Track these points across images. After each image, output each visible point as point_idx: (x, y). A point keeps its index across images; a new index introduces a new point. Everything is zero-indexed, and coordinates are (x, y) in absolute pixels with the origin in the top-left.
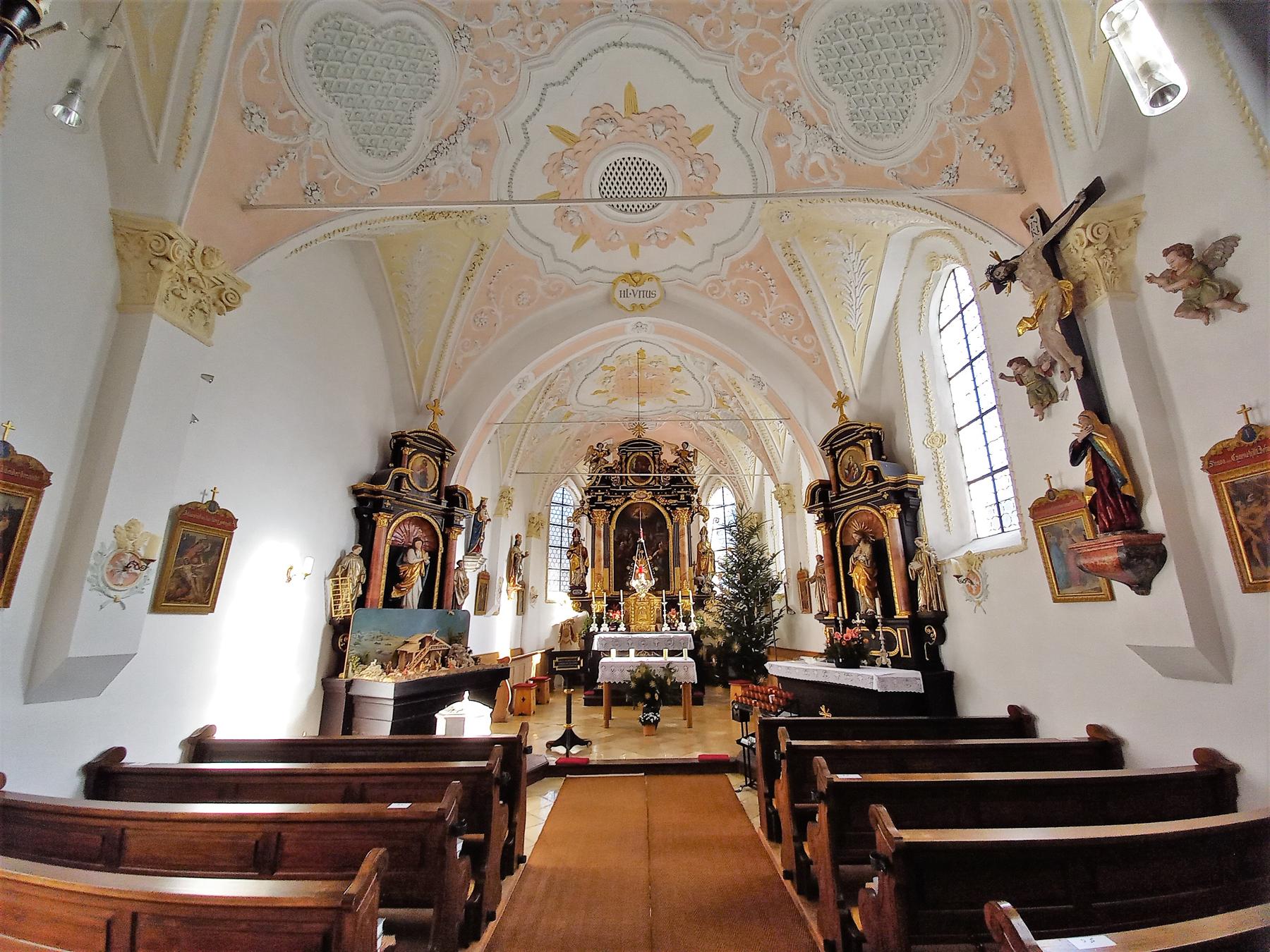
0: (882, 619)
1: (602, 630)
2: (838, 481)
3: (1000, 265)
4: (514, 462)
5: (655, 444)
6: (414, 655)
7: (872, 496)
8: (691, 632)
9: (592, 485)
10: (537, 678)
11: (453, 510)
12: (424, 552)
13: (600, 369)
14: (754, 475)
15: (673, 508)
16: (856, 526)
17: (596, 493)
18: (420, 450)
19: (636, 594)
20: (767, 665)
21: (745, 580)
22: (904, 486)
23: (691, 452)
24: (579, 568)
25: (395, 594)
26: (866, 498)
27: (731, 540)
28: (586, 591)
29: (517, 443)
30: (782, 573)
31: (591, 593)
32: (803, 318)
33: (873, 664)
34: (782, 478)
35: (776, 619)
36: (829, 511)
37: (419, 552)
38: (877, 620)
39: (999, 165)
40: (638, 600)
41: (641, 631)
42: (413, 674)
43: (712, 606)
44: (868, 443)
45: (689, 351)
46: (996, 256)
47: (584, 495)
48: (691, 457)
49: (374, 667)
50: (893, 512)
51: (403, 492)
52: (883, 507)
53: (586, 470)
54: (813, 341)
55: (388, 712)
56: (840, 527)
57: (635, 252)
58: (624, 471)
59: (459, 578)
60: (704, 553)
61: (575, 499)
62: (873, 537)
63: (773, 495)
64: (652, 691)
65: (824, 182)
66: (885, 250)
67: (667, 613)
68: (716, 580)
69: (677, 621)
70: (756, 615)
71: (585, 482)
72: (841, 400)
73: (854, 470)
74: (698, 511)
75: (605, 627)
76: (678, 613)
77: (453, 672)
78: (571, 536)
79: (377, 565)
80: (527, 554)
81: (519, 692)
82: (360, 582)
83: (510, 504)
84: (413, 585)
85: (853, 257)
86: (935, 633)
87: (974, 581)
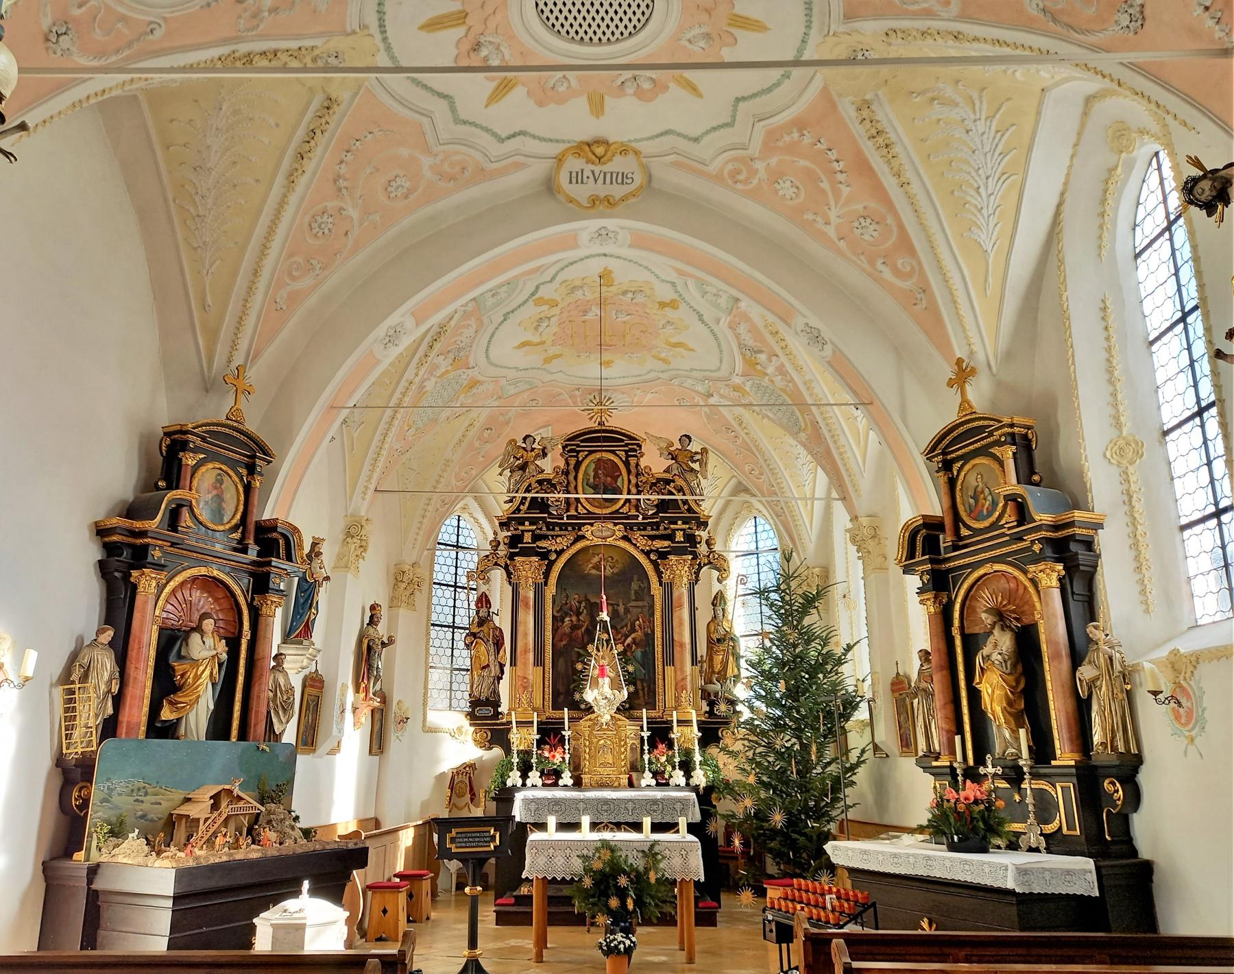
0: (1031, 767)
1: (529, 782)
2: (957, 519)
3: (1204, 177)
4: (372, 471)
5: (631, 438)
6: (202, 822)
7: (1015, 547)
8: (696, 789)
9: (514, 513)
10: (406, 873)
11: (269, 564)
12: (217, 638)
13: (531, 303)
14: (813, 499)
15: (663, 555)
16: (986, 599)
17: (520, 528)
18: (212, 457)
19: (593, 716)
20: (829, 847)
21: (794, 693)
22: (1070, 531)
23: (696, 453)
24: (488, 665)
25: (166, 714)
26: (1004, 550)
27: (770, 617)
28: (500, 710)
29: (378, 437)
30: (863, 681)
31: (509, 714)
32: (895, 229)
33: (1013, 846)
34: (862, 506)
35: (853, 768)
36: (940, 571)
37: (209, 641)
38: (1021, 768)
39: (1207, 8)
40: (597, 728)
41: (602, 786)
42: (201, 855)
43: (734, 740)
44: (1008, 452)
45: (691, 276)
46: (1197, 163)
47: (498, 529)
48: (695, 461)
49: (134, 843)
50: (1050, 576)
51: (183, 533)
52: (1032, 568)
53: (502, 483)
54: (912, 267)
55: (162, 921)
56: (959, 600)
57: (597, 107)
58: (572, 488)
59: (276, 682)
60: (719, 640)
61: (481, 537)
62: (1017, 620)
63: (848, 535)
64: (622, 894)
65: (925, 9)
66: (1039, 113)
67: (649, 753)
68: (741, 692)
69: (669, 768)
70: (813, 757)
71: (501, 508)
72: (963, 374)
73: (985, 499)
74: (710, 563)
75: (534, 777)
76: (670, 753)
77: (273, 851)
78: (473, 606)
79: (138, 660)
80: (391, 641)
81: (378, 896)
82: (109, 691)
83: (363, 548)
84: (198, 697)
85: (981, 126)
86: (1121, 792)
87: (1184, 701)
